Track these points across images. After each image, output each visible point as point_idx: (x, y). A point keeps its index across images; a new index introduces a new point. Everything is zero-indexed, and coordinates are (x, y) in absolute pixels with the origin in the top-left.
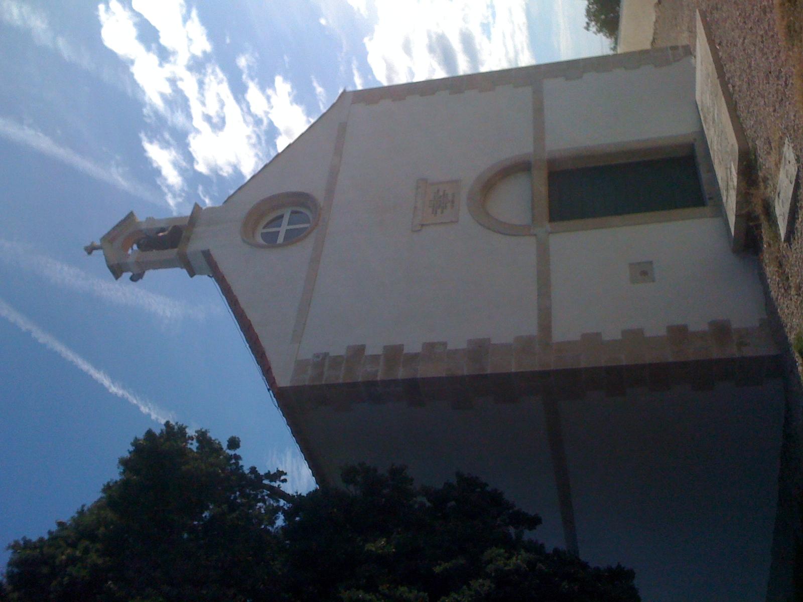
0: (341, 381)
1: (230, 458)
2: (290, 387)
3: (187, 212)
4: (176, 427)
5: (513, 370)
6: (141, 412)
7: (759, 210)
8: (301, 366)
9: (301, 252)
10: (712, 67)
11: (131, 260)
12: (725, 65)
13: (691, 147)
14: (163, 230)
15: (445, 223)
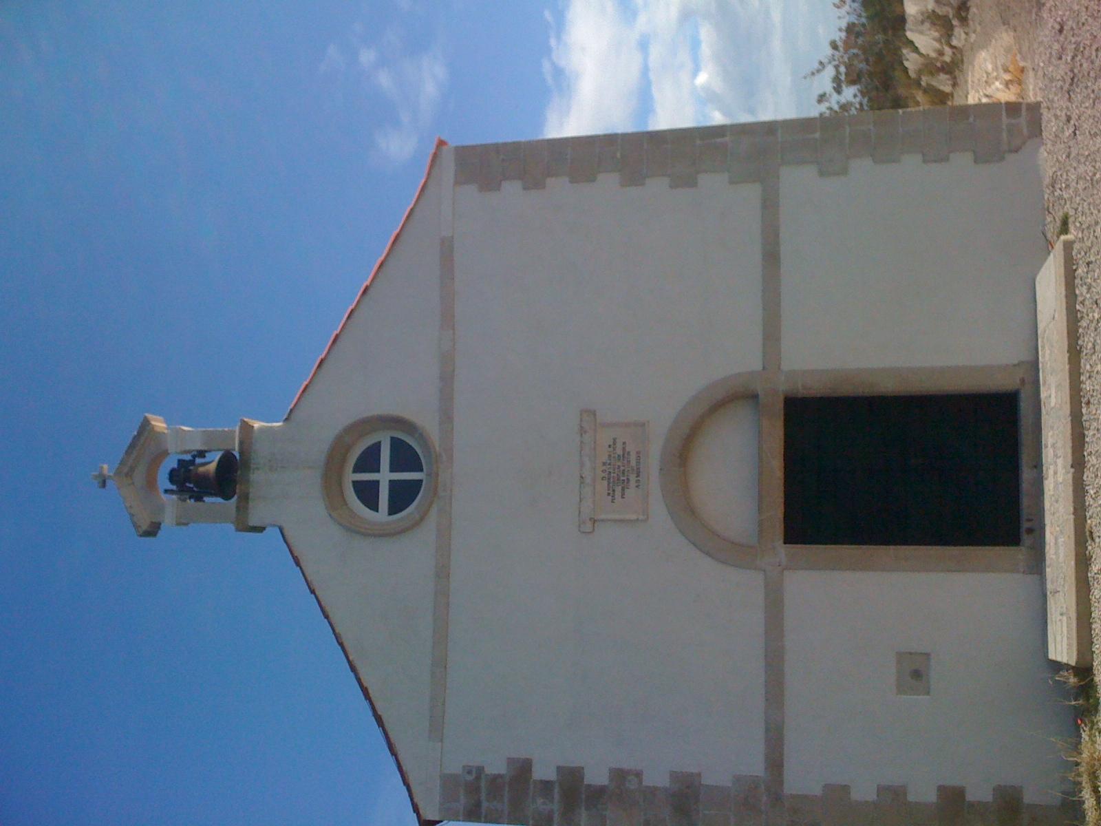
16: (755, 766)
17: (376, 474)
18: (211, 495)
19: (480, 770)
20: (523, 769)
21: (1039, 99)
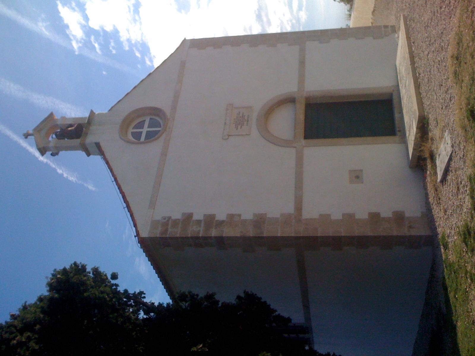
0: (178, 235)
1: (113, 285)
3: (87, 115)
4: (80, 265)
5: (279, 235)
6: (57, 173)
7: (427, 155)
8: (155, 224)
9: (156, 147)
10: (407, 56)
11: (51, 145)
12: (416, 57)
13: (391, 95)
14: (71, 126)
15: (242, 135)
16: (290, 209)
18: (106, 113)
19: (170, 218)
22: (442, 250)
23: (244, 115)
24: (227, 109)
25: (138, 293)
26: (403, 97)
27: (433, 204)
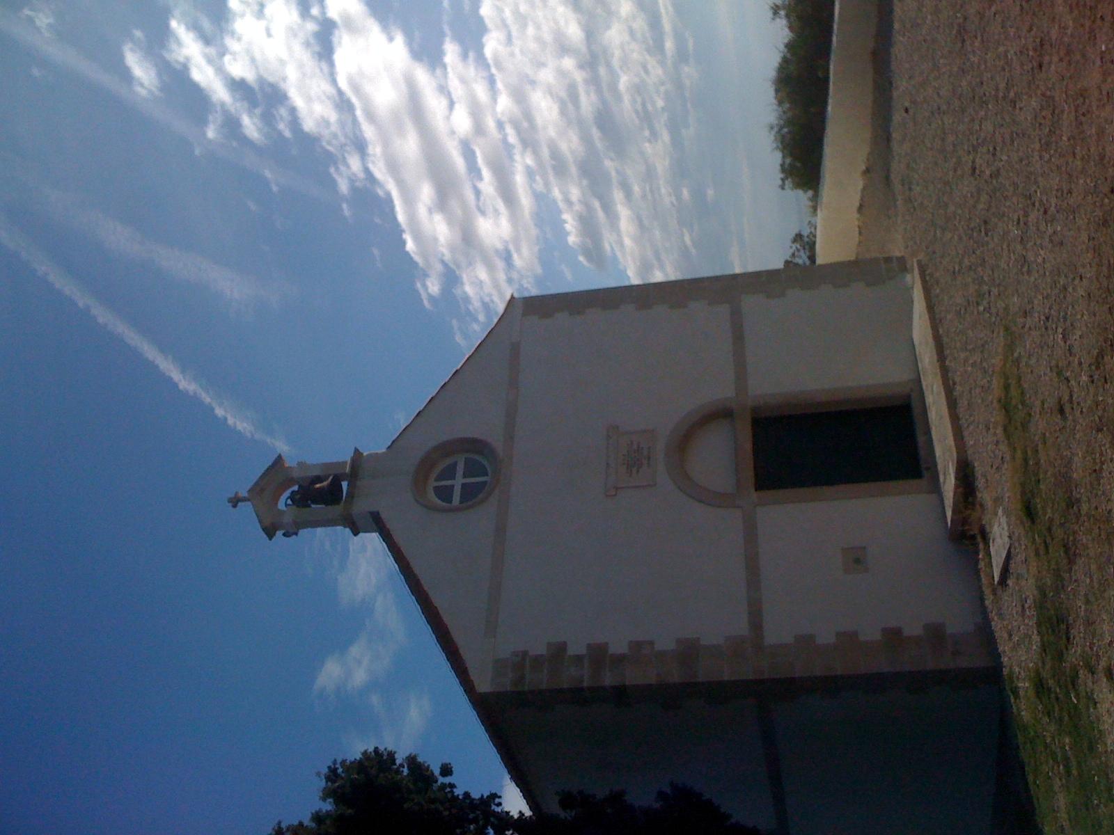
0: (544, 686)
1: (444, 786)
2: (490, 693)
4: (385, 754)
5: (726, 678)
13: (909, 396)
14: (319, 479)
16: (741, 627)
17: (453, 481)
18: (384, 453)
19: (525, 653)
20: (561, 648)
21: (903, 254)
22: (1013, 700)
23: (641, 446)
24: (608, 436)
25: (487, 797)
26: (930, 406)
27: (992, 612)
